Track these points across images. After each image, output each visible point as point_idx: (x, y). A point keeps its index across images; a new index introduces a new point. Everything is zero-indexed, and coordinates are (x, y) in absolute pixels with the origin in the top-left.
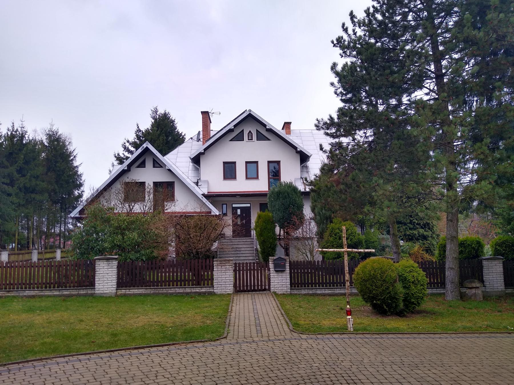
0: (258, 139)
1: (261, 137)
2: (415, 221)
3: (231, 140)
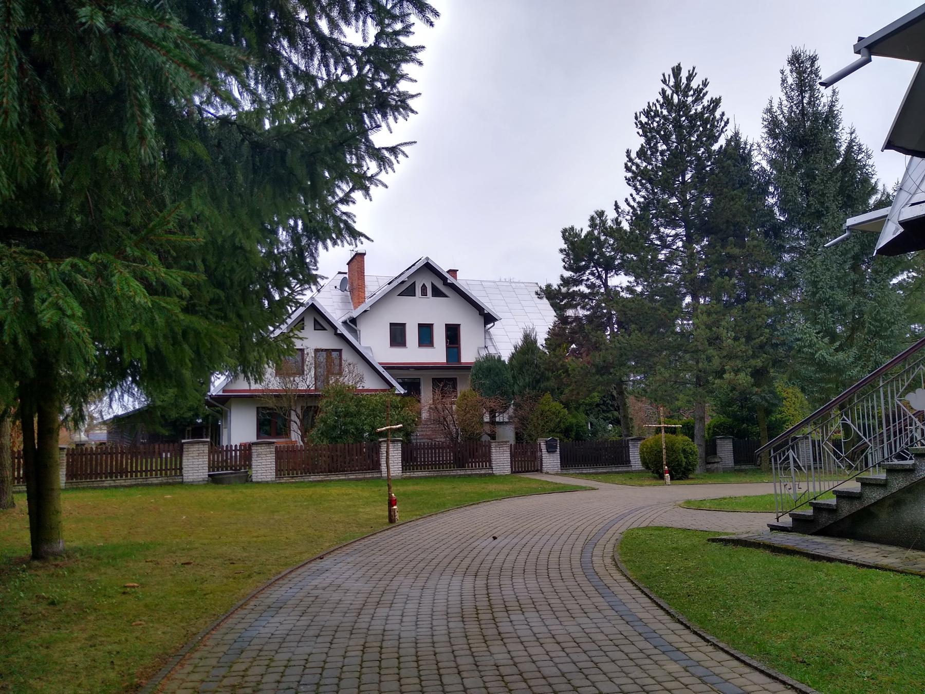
0: (433, 296)
1: (437, 293)
2: (609, 401)
3: (399, 295)
